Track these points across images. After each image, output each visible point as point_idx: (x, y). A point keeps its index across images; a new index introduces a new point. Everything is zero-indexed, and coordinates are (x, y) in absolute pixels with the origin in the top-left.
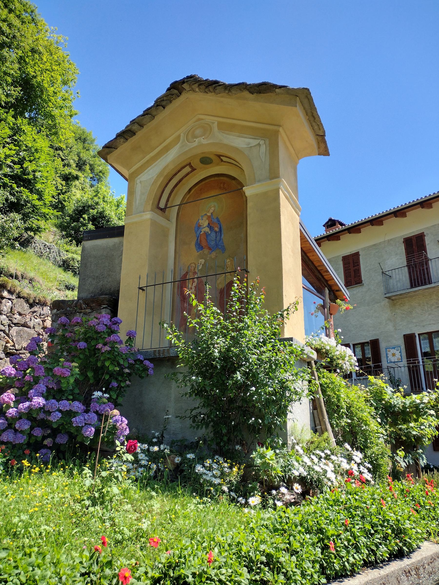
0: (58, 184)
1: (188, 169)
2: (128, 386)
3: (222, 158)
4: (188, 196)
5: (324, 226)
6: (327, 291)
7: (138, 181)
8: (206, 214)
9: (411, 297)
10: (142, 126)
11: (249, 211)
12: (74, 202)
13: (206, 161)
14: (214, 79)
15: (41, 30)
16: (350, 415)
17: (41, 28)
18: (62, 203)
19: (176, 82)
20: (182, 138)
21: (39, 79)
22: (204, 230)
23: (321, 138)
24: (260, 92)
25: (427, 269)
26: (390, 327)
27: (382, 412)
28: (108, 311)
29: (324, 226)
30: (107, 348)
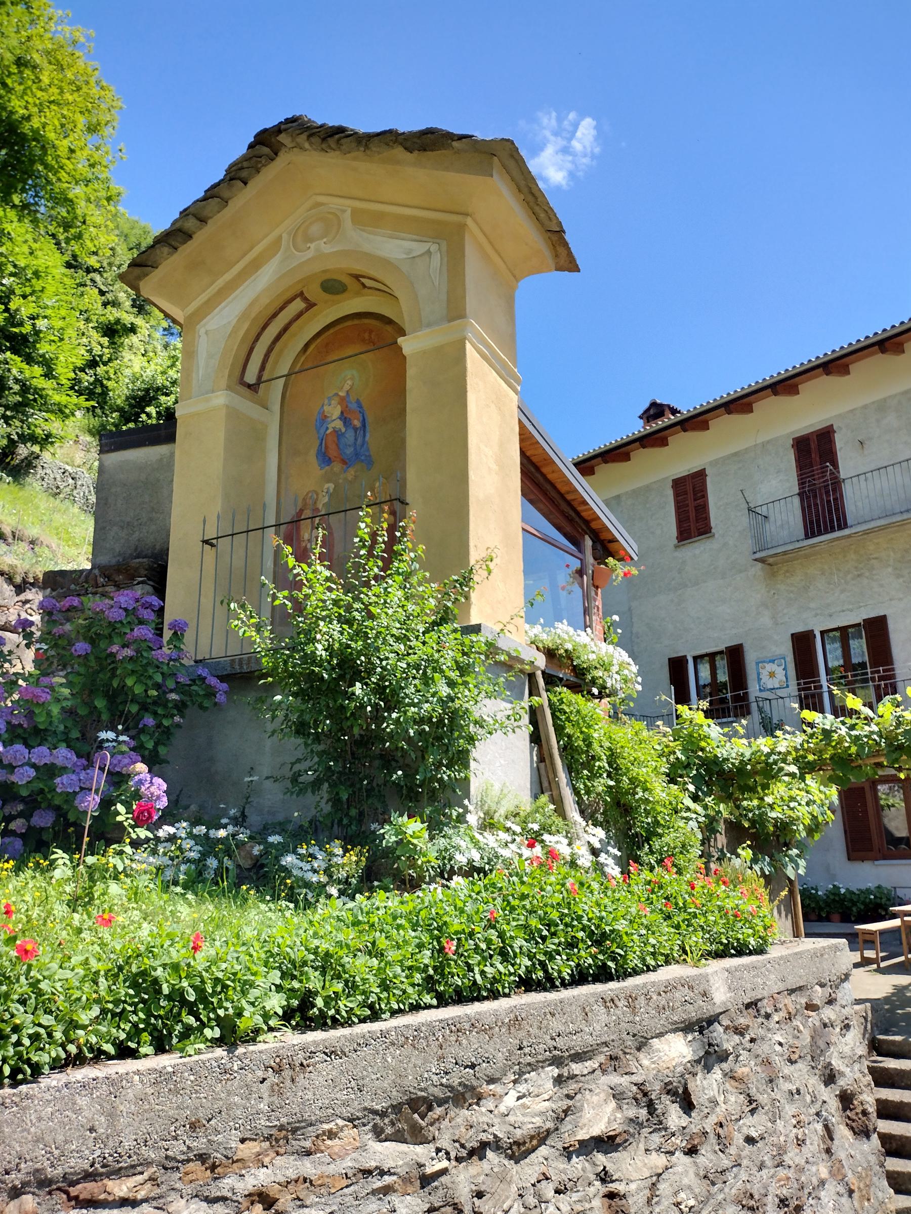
0: (94, 344)
1: (298, 305)
2: (178, 726)
3: (362, 280)
4: (303, 359)
5: (641, 417)
6: (588, 542)
7: (202, 331)
8: (337, 394)
9: (806, 557)
10: (203, 221)
11: (409, 384)
12: (127, 380)
13: (333, 287)
14: (336, 124)
15: (39, 17)
16: (615, 771)
17: (38, 13)
18: (102, 385)
19: (265, 131)
20: (284, 242)
21: (36, 123)
22: (333, 425)
23: (556, 236)
24: (423, 149)
25: (835, 499)
26: (766, 620)
27: (700, 774)
28: (148, 588)
29: (641, 417)
30: (128, 652)
